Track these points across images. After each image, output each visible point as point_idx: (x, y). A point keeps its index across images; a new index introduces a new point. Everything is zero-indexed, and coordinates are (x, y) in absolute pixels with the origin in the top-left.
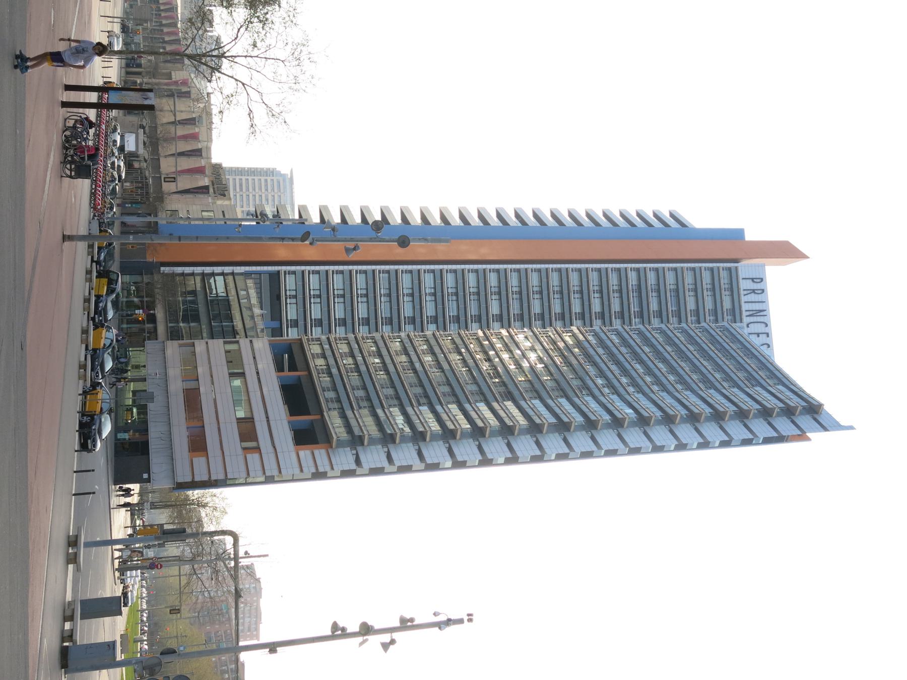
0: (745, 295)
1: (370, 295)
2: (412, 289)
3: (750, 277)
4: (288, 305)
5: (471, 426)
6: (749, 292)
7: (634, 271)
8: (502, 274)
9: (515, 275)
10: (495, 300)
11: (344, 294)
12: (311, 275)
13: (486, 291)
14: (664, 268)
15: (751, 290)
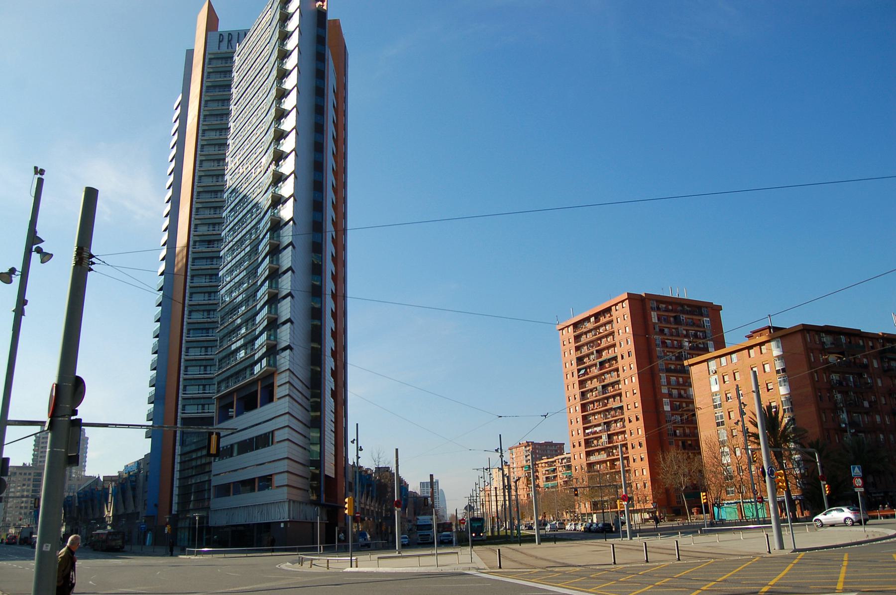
0: (232, 48)
1: (203, 383)
2: (201, 347)
3: (218, 43)
4: (209, 411)
5: (264, 358)
6: (229, 45)
7: (197, 229)
8: (194, 290)
9: (196, 280)
10: (215, 297)
11: (203, 385)
12: (187, 392)
13: (201, 398)
14: (188, 323)
15: (228, 44)
